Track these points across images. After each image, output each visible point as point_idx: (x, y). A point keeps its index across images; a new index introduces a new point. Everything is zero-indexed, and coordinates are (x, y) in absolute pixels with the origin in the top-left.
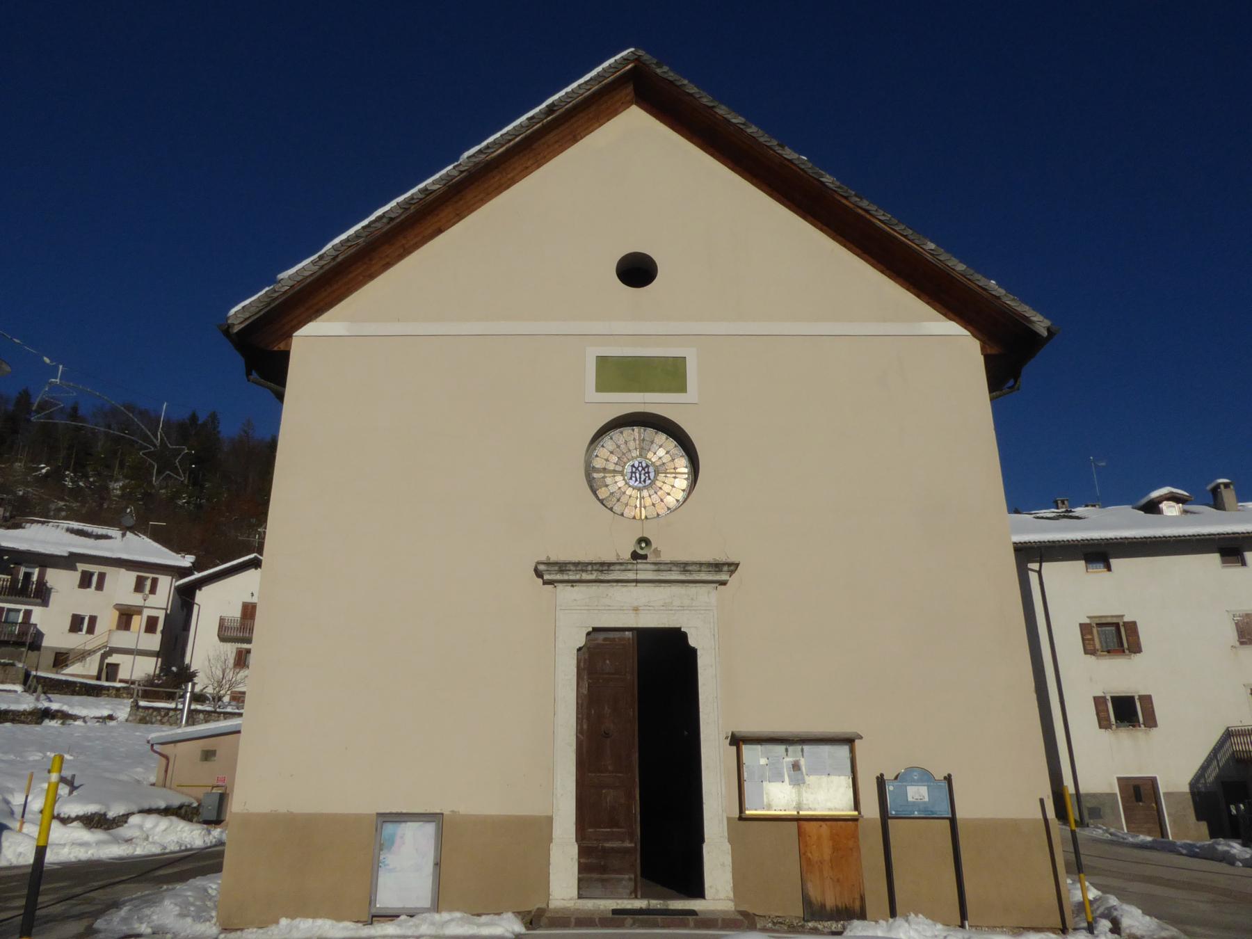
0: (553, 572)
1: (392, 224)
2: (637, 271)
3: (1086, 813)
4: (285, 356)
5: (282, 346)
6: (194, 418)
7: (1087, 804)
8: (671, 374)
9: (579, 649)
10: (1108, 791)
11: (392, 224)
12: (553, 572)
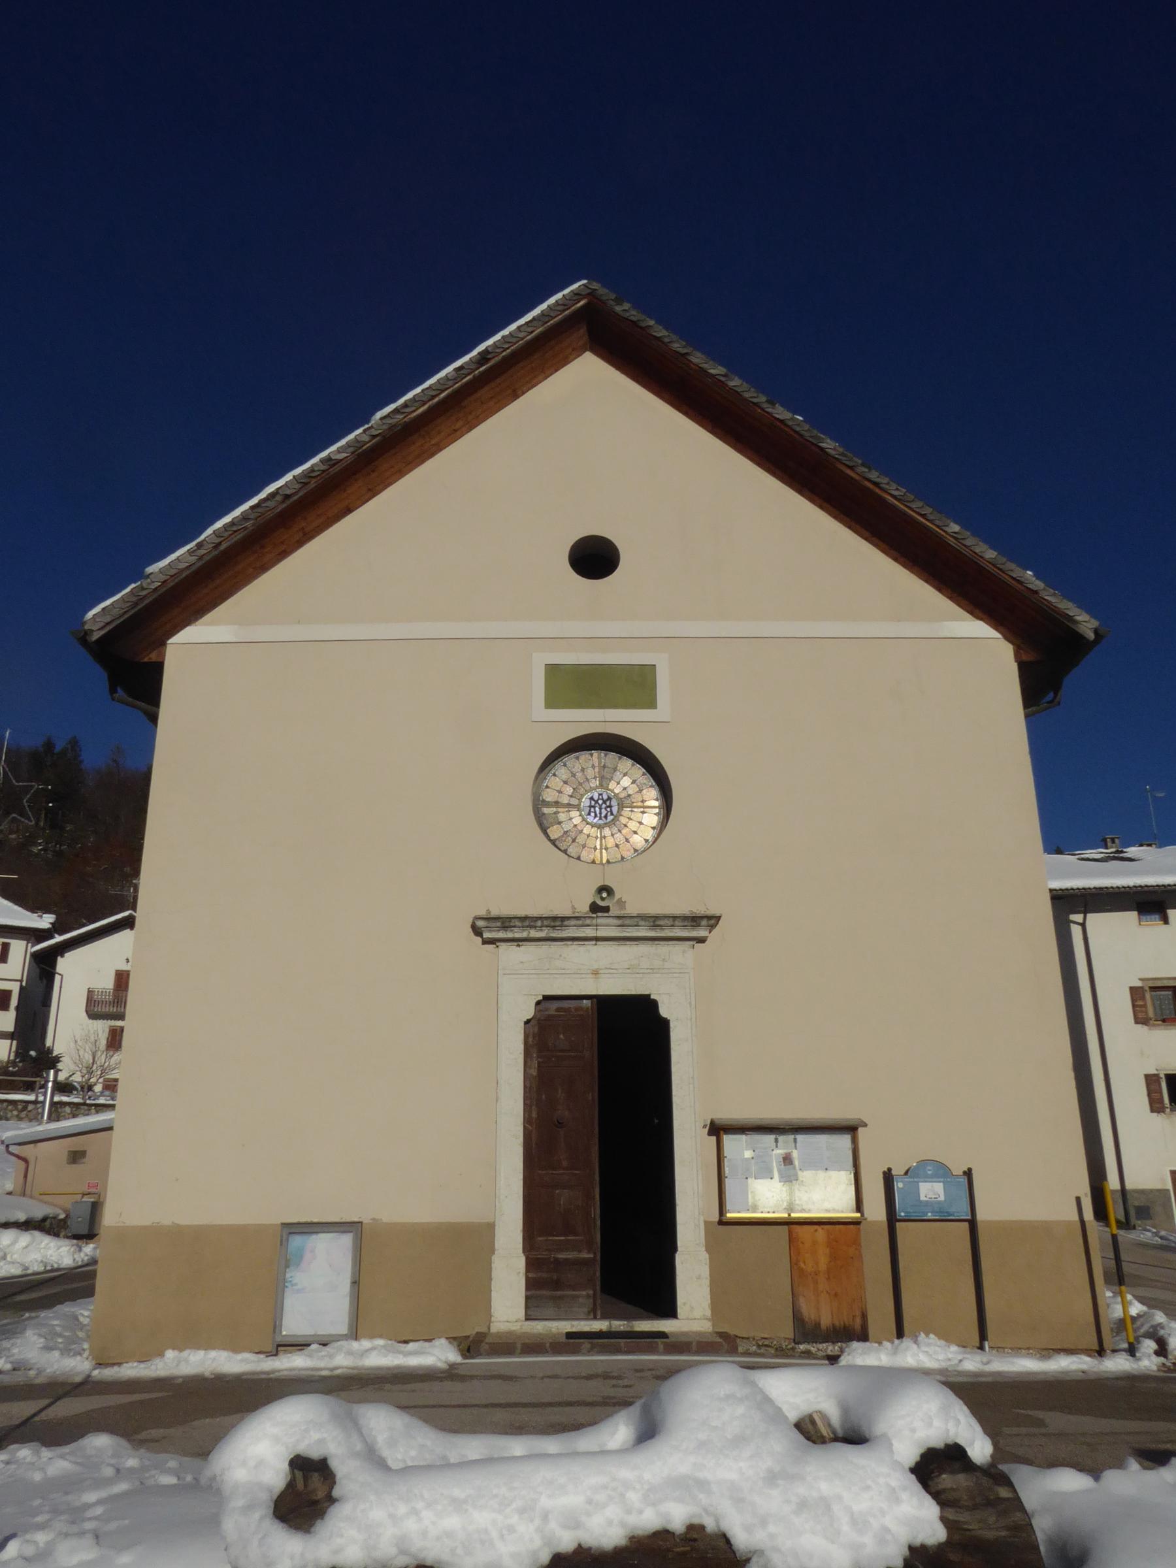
0: (494, 929)
1: (288, 502)
2: (594, 558)
3: (1132, 1212)
4: (157, 670)
5: (153, 657)
6: (49, 745)
7: (1134, 1202)
8: (636, 685)
9: (527, 1022)
10: (1159, 1187)
11: (288, 502)
12: (494, 929)
